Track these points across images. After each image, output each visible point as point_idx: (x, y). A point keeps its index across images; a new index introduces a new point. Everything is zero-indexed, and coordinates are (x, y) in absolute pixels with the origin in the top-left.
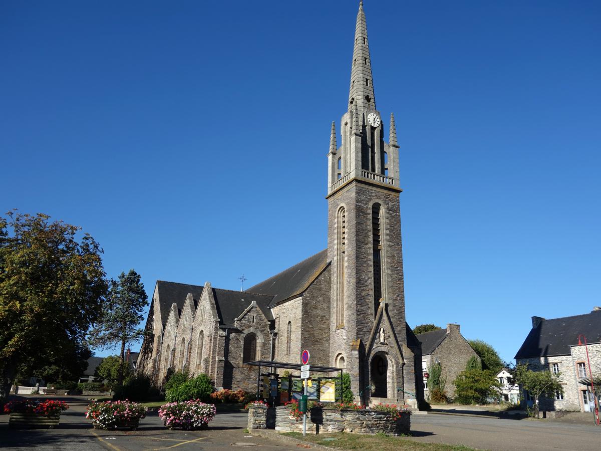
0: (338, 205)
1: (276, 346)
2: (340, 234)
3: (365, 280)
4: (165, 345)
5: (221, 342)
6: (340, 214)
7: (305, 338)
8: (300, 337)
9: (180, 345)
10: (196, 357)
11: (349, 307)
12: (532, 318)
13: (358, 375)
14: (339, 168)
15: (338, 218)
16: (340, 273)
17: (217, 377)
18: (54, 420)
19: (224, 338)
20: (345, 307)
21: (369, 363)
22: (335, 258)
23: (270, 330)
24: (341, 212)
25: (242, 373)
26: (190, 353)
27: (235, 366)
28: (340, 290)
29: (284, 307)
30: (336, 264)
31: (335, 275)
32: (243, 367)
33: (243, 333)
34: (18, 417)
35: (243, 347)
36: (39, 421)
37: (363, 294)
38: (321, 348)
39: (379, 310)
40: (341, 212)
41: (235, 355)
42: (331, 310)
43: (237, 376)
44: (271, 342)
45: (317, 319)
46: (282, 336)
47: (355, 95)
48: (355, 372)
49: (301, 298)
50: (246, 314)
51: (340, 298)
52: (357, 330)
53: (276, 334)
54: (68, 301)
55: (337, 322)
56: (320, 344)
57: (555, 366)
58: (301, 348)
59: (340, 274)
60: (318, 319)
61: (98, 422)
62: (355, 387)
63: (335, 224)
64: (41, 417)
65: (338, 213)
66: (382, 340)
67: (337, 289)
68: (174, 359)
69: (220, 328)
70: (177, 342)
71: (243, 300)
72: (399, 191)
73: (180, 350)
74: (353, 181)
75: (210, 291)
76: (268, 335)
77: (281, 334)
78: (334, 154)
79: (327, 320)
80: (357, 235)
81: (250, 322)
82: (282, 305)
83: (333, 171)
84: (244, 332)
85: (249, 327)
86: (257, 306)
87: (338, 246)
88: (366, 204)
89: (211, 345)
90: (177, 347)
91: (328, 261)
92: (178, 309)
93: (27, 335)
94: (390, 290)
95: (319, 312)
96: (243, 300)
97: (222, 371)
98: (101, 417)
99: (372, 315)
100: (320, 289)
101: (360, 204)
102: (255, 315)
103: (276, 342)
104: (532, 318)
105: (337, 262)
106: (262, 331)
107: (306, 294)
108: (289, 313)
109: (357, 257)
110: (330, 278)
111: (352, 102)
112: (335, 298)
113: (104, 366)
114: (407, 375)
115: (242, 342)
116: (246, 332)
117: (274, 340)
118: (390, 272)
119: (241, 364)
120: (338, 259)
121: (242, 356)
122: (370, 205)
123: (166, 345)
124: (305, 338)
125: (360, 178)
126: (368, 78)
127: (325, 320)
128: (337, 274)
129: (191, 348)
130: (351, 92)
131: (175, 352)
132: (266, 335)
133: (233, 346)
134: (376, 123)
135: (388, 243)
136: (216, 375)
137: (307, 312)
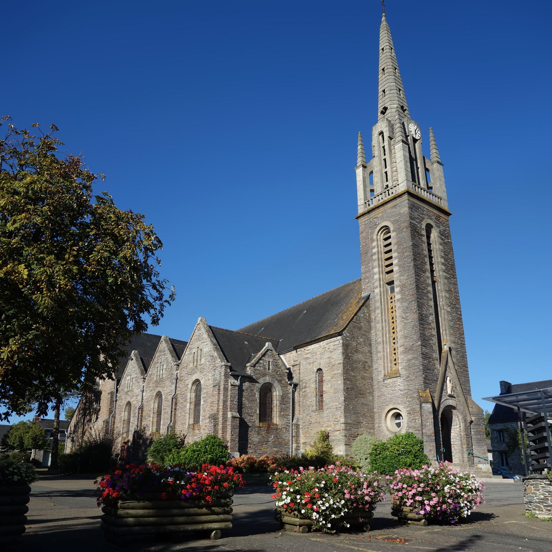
0: (376, 225)
1: (296, 401)
2: (382, 261)
3: (427, 316)
4: (122, 402)
5: (232, 393)
6: (380, 236)
7: (348, 388)
8: (342, 387)
9: (153, 401)
10: (187, 415)
11: (407, 350)
12: (500, 382)
13: (433, 435)
14: (372, 183)
15: (377, 241)
16: (385, 309)
17: (231, 440)
18: (222, 517)
19: (237, 388)
20: (401, 349)
21: (440, 420)
22: (377, 291)
23: (289, 380)
24: (381, 233)
25: (259, 434)
26: (175, 409)
27: (250, 424)
28: (386, 330)
29: (307, 352)
30: (378, 297)
31: (378, 311)
32: (259, 427)
33: (257, 382)
34: (141, 512)
35: (258, 401)
36: (192, 520)
37: (426, 333)
38: (365, 402)
39: (443, 355)
40: (381, 233)
41: (250, 411)
42: (374, 356)
43: (253, 437)
44: (291, 395)
45: (359, 366)
46: (305, 387)
47: (389, 103)
48: (429, 430)
49: (339, 337)
50: (260, 359)
51: (386, 339)
52: (425, 378)
53: (296, 386)
54: (110, 281)
55: (384, 370)
56: (363, 397)
57: (500, 434)
58: (345, 401)
59: (385, 312)
60: (360, 366)
61: (315, 515)
62: (430, 450)
63: (374, 248)
64: (192, 510)
65: (377, 235)
66: (449, 392)
67: (383, 329)
68: (141, 419)
69: (231, 375)
70: (145, 398)
71: (246, 343)
72: (448, 214)
73: (152, 407)
74: (404, 194)
75: (208, 328)
76: (287, 387)
77: (302, 385)
78: (364, 167)
79: (369, 367)
80: (415, 260)
81: (265, 369)
82: (303, 349)
83: (365, 186)
84: (259, 381)
85: (264, 375)
86: (273, 349)
87: (379, 275)
88: (419, 223)
89: (219, 397)
90: (145, 404)
91: (364, 294)
92: (141, 358)
93: (29, 344)
94: (452, 332)
95: (360, 356)
96: (246, 343)
97: (237, 430)
98: (323, 504)
99: (437, 360)
100: (360, 328)
101: (414, 222)
102: (271, 360)
103: (296, 395)
104: (500, 382)
105: (381, 295)
106: (280, 381)
107: (345, 333)
108: (326, 354)
109: (418, 287)
110: (369, 315)
111: (383, 113)
112: (380, 340)
113: (15, 434)
114: (476, 435)
115: (257, 393)
116: (262, 381)
117: (293, 393)
118: (449, 309)
119: (257, 423)
120: (380, 292)
121: (258, 412)
122: (424, 226)
123: (124, 402)
124: (348, 388)
125: (412, 191)
126: (401, 88)
127: (367, 367)
128: (381, 310)
129: (176, 404)
130: (380, 102)
131: (142, 411)
132: (284, 387)
133: (247, 399)
134: (417, 134)
135: (445, 274)
136: (229, 436)
137: (348, 356)
